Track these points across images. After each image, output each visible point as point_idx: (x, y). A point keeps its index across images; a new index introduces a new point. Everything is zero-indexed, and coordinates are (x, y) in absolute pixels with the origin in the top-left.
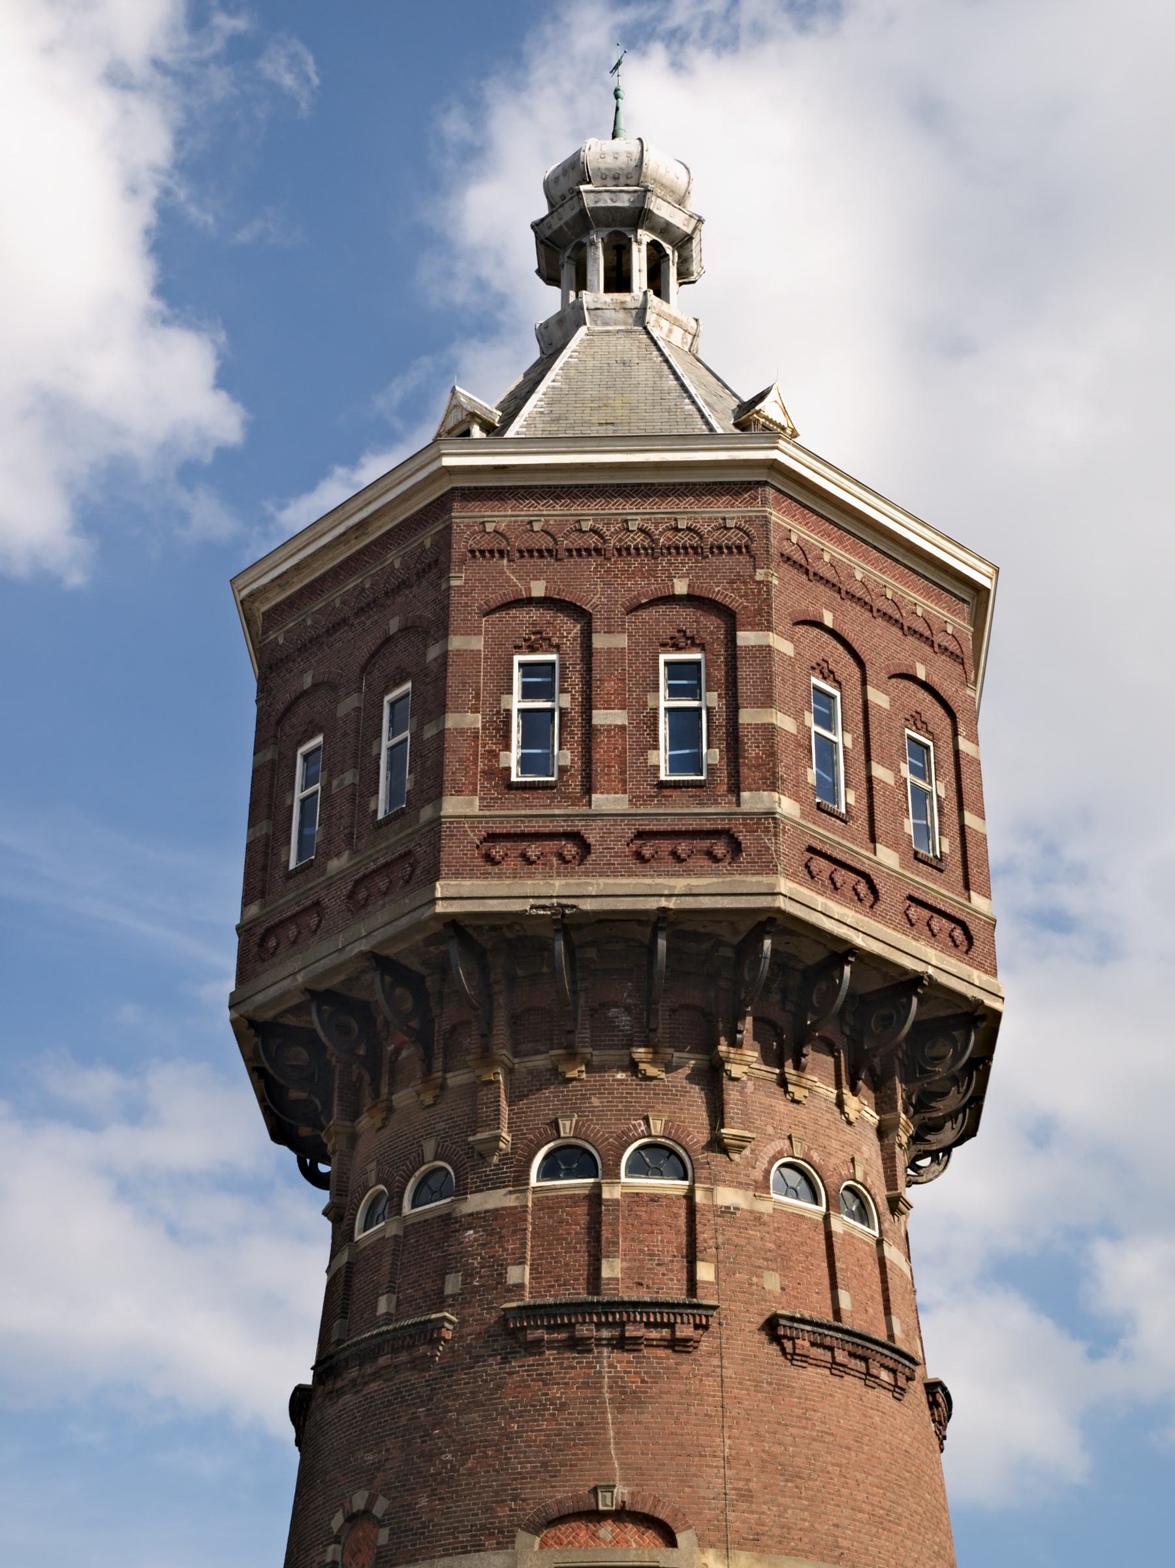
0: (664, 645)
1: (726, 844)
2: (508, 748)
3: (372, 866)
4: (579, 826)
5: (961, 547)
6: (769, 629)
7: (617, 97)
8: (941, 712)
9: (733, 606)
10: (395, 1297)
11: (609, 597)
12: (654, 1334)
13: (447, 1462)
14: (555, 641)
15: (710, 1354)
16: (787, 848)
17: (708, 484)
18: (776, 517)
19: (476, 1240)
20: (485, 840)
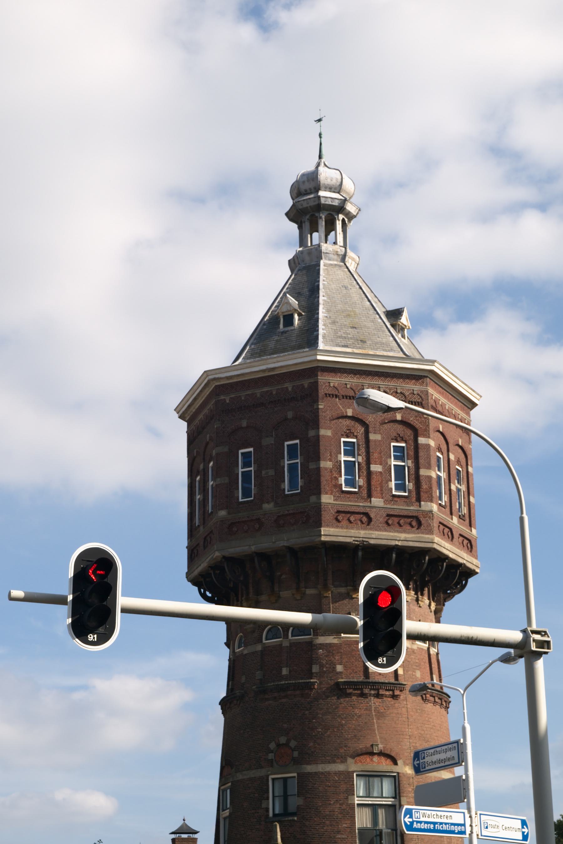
0: (392, 439)
1: (417, 522)
2: (341, 476)
3: (286, 512)
4: (368, 510)
5: (474, 391)
6: (429, 437)
7: (320, 137)
8: (463, 456)
9: (417, 426)
10: (288, 668)
11: (374, 419)
12: (387, 693)
13: (319, 732)
14: (355, 434)
15: (403, 700)
16: (327, 516)
17: (407, 375)
18: (431, 391)
19: (323, 654)
20: (336, 513)
